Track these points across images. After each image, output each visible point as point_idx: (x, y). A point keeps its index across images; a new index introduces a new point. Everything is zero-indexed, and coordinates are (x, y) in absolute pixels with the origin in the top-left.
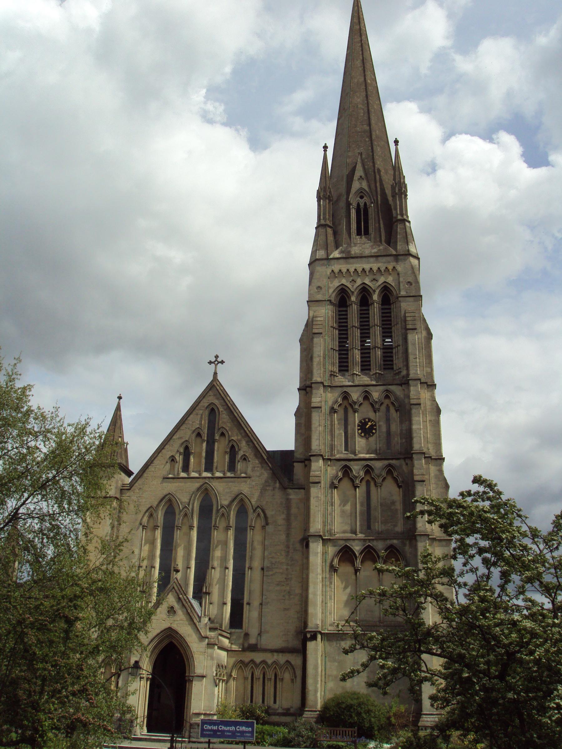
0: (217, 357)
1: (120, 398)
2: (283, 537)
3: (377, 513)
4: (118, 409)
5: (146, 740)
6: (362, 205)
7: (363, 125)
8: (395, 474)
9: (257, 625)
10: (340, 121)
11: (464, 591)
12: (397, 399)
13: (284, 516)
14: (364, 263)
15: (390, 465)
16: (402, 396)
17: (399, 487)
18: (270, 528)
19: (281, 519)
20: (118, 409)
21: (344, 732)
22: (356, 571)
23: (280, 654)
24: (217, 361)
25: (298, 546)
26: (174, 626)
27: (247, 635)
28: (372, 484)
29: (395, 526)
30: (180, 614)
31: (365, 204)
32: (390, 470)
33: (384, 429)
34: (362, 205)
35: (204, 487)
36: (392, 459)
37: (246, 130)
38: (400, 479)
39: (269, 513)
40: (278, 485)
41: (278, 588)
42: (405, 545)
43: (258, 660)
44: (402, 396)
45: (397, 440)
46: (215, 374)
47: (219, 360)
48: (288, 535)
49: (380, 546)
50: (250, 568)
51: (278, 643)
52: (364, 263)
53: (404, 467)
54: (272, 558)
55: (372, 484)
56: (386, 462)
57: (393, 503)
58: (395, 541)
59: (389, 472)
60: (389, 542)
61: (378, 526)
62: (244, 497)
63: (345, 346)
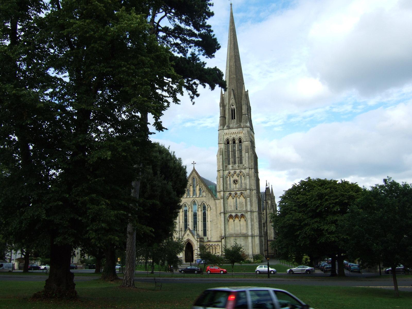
0: (194, 162)
2: (215, 213)
3: (238, 206)
5: (185, 264)
6: (233, 109)
7: (233, 75)
8: (243, 195)
9: (210, 235)
10: (227, 71)
12: (243, 173)
13: (215, 207)
14: (235, 133)
15: (241, 192)
16: (245, 172)
17: (244, 198)
18: (211, 211)
19: (214, 208)
21: (228, 146)
22: (234, 221)
23: (216, 242)
25: (219, 215)
26: (189, 238)
27: (208, 238)
28: (237, 197)
29: (243, 209)
30: (191, 235)
31: (234, 108)
32: (241, 194)
33: (240, 182)
34: (233, 109)
35: (194, 200)
36: (242, 191)
37: (182, 166)
38: (244, 196)
40: (213, 199)
41: (215, 226)
42: (245, 214)
43: (211, 244)
44: (245, 172)
45: (243, 185)
47: (195, 163)
48: (216, 212)
49: (239, 214)
50: (207, 221)
51: (215, 240)
52: (235, 133)
53: (245, 193)
54: (213, 218)
55: (237, 197)
57: (243, 202)
58: (243, 213)
59: (241, 194)
60: (242, 213)
61: (239, 209)
62: (204, 202)
63: (229, 164)
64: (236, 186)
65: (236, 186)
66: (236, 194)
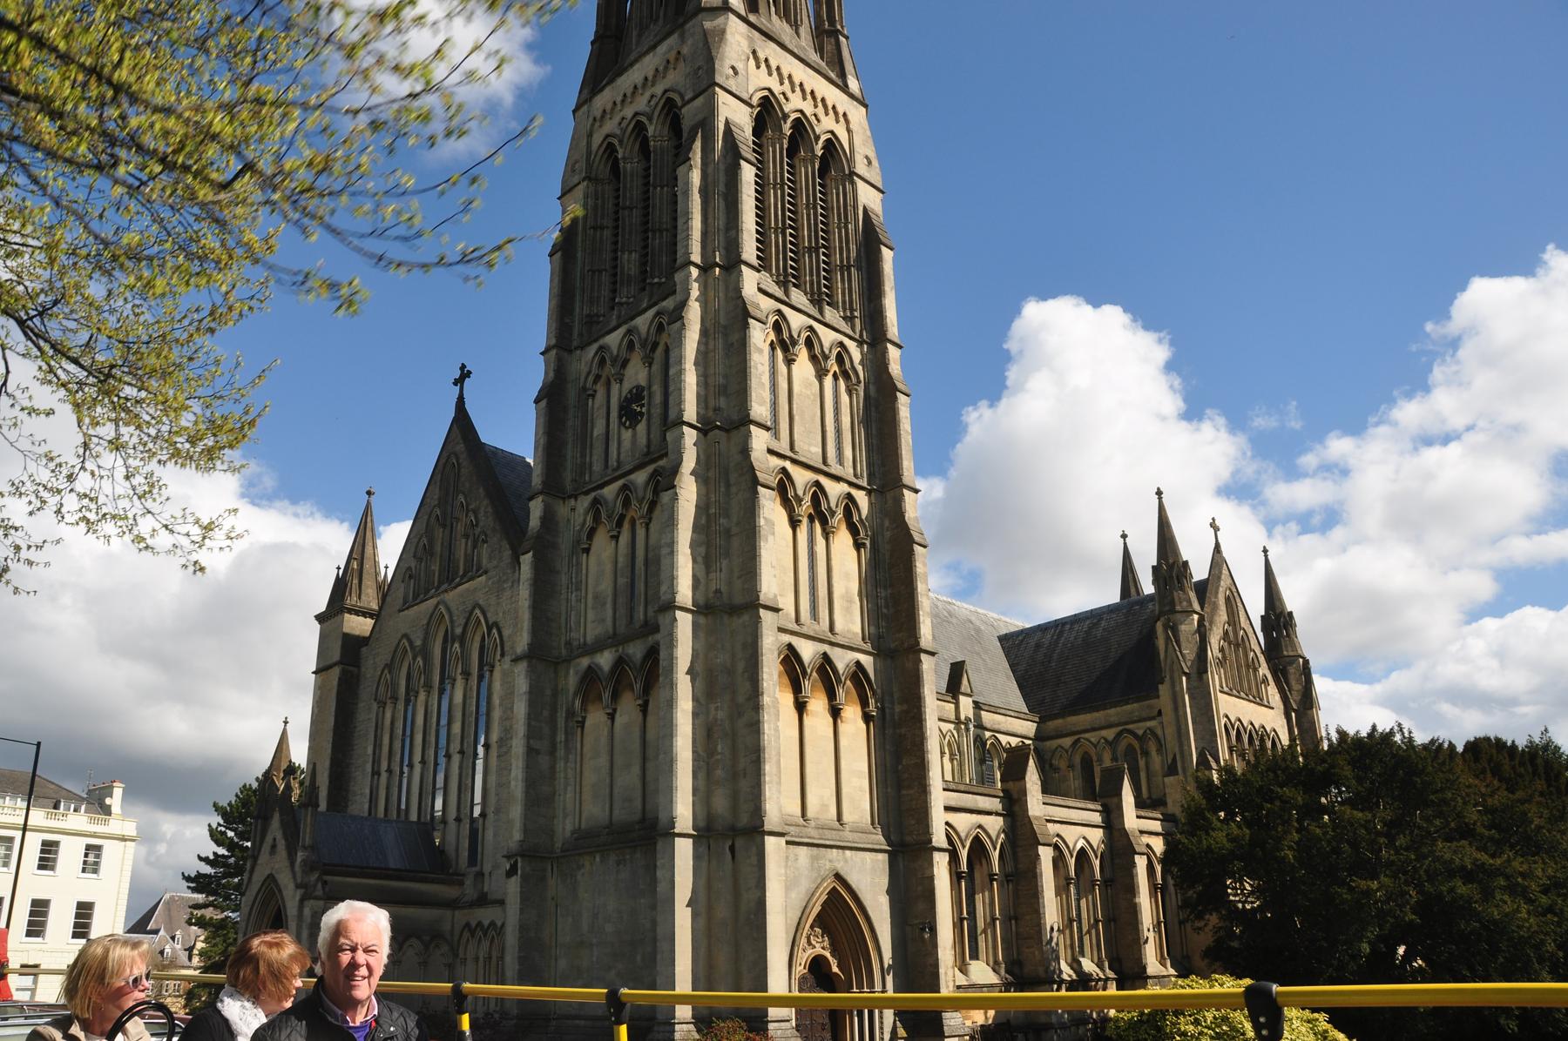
1: (369, 493)
4: (368, 507)
11: (562, 510)
20: (368, 507)
24: (465, 374)
33: (658, 398)
39: (506, 633)
46: (461, 402)
56: (620, 483)
64: (634, 435)
65: (634, 435)
66: (627, 503)
